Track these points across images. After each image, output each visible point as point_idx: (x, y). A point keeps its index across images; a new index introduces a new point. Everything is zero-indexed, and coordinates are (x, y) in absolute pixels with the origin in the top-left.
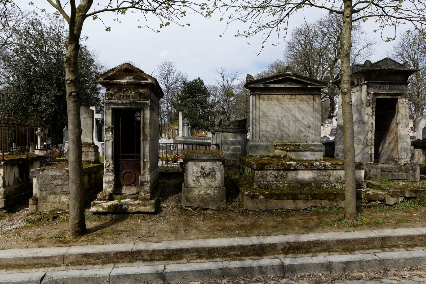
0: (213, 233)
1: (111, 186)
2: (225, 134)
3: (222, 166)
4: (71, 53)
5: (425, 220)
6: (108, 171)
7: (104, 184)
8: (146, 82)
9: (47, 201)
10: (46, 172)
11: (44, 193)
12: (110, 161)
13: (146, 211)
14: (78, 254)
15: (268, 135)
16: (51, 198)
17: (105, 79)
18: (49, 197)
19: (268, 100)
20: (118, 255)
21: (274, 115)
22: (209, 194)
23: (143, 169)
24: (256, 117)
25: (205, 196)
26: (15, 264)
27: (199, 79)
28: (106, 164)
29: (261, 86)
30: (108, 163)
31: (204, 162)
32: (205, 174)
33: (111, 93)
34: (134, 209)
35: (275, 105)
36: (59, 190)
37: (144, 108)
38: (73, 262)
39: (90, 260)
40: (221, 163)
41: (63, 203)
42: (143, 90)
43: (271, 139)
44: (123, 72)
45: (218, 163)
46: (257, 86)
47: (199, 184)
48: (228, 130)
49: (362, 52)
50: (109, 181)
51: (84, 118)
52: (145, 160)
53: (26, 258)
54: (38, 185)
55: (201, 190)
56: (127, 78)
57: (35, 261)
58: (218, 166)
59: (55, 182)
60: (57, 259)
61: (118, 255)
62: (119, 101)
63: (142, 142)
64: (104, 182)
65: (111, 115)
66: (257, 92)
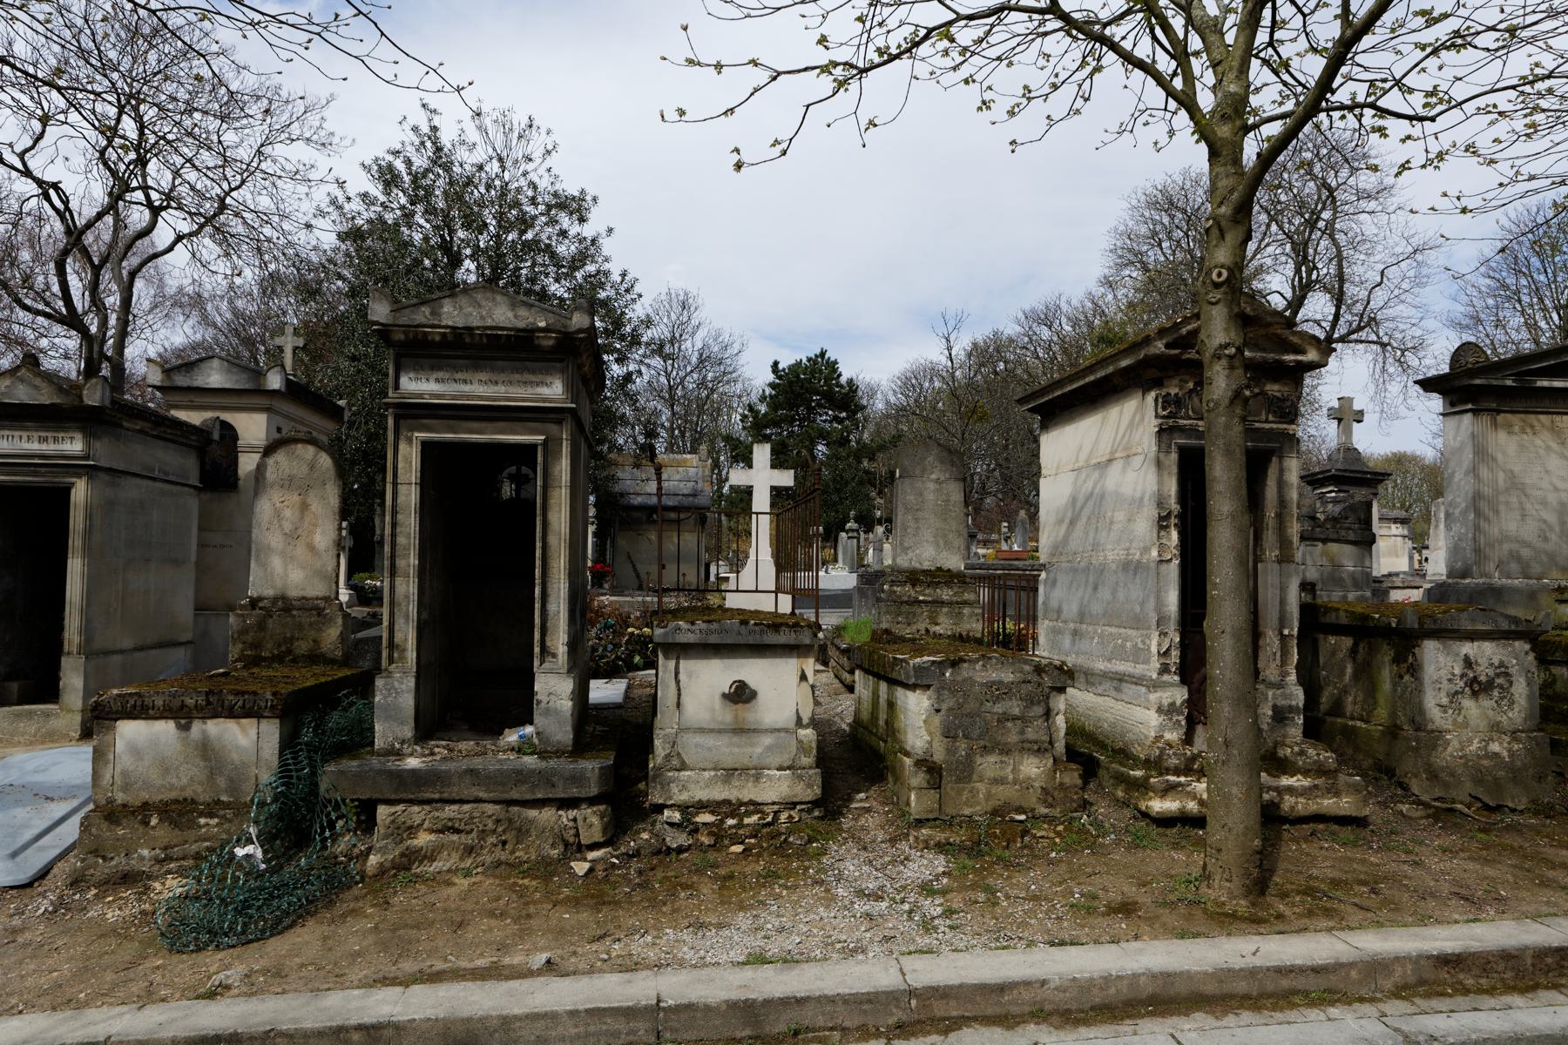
0: (1474, 903)
2: (1334, 547)
3: (1531, 657)
5: (1543, 882)
8: (1300, 358)
9: (975, 777)
10: (965, 671)
11: (962, 746)
12: (1171, 634)
13: (1343, 813)
14: (1420, 957)
15: (1526, 553)
16: (988, 765)
17: (1167, 346)
18: (979, 760)
19: (1523, 431)
20: (1549, 960)
21: (1545, 484)
22: (1496, 755)
24: (1486, 491)
25: (1485, 762)
26: (1217, 992)
27: (823, 354)
29: (1509, 383)
31: (1472, 640)
32: (1480, 683)
34: (1302, 806)
35: (1548, 448)
36: (1013, 738)
37: (1281, 448)
38: (1405, 987)
39: (1461, 976)
40: (1527, 647)
41: (1027, 785)
42: (1276, 387)
43: (1536, 569)
45: (1522, 646)
46: (1495, 383)
47: (1460, 719)
48: (1343, 533)
49: (1390, 273)
50: (1173, 704)
51: (937, 481)
52: (1286, 632)
53: (1252, 973)
54: (937, 720)
55: (1470, 741)
57: (1285, 983)
58: (1517, 656)
59: (999, 708)
60: (1354, 973)
61: (1549, 960)
65: (1175, 470)
66: (1486, 405)
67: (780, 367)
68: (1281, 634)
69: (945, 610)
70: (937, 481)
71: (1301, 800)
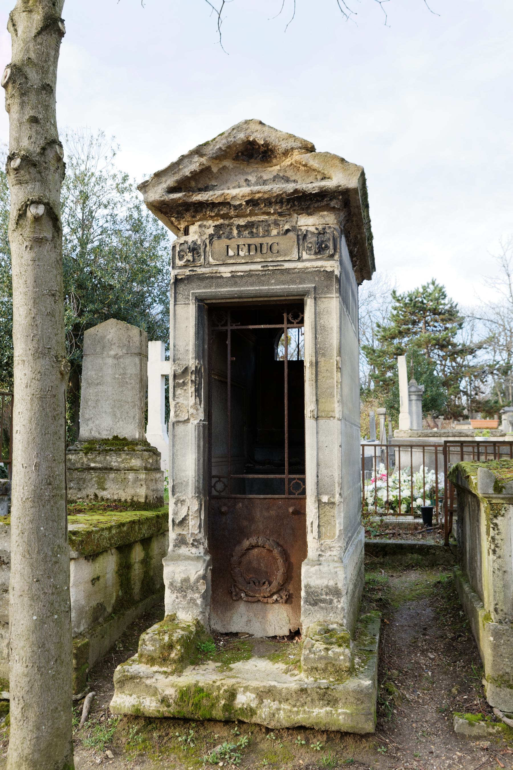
1: (192, 601)
4: (28, 51)
6: (181, 541)
7: (167, 592)
12: (188, 503)
23: (315, 534)
28: (175, 514)
30: (185, 508)
33: (194, 243)
44: (236, 158)
50: (186, 580)
51: (116, 357)
52: (325, 499)
56: (252, 178)
62: (222, 269)
63: (309, 424)
64: (166, 583)
67: (398, 294)
68: (319, 501)
69: (112, 475)
70: (116, 357)
71: (285, 706)
